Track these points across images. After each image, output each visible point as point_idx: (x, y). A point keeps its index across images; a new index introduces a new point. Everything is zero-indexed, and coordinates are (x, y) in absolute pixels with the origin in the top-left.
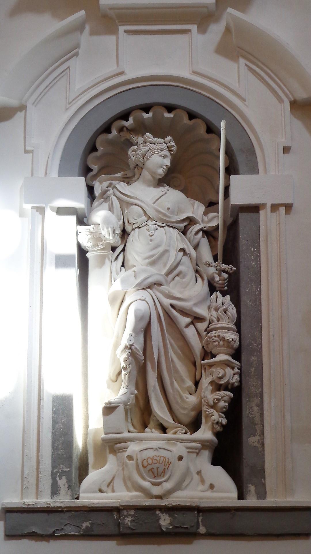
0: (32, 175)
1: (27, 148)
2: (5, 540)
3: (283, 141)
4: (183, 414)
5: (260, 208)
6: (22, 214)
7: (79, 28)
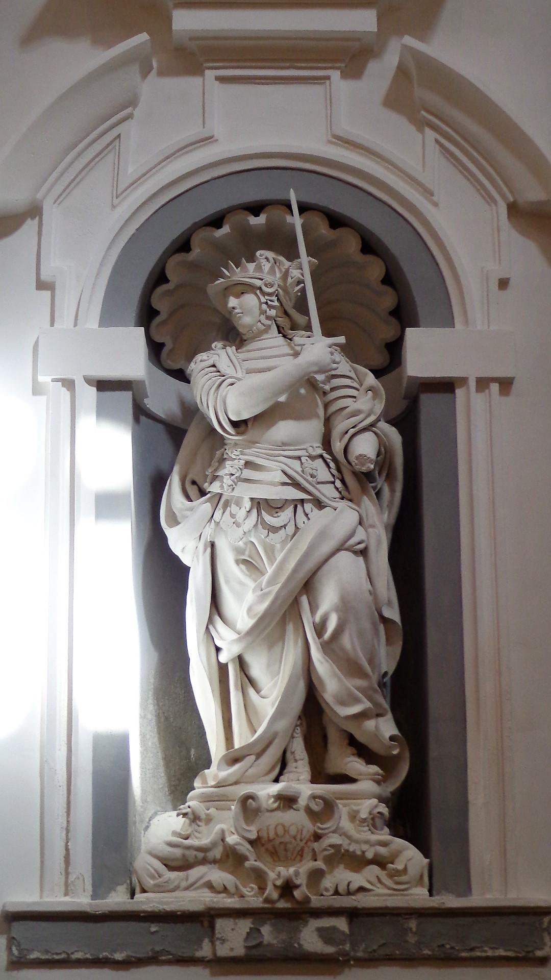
0: (52, 324)
3: (498, 271)
5: (456, 385)
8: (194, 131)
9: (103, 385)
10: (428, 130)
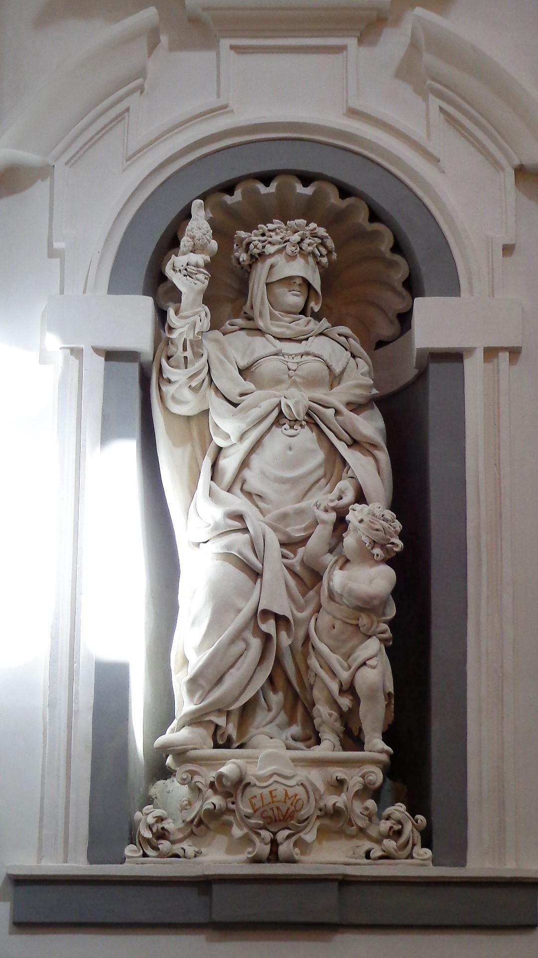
0: (62, 292)
1: (57, 245)
2: (11, 933)
3: (501, 238)
4: (266, 747)
6: (44, 359)
7: (153, 37)
8: (213, 101)
9: (111, 355)
10: (431, 97)
